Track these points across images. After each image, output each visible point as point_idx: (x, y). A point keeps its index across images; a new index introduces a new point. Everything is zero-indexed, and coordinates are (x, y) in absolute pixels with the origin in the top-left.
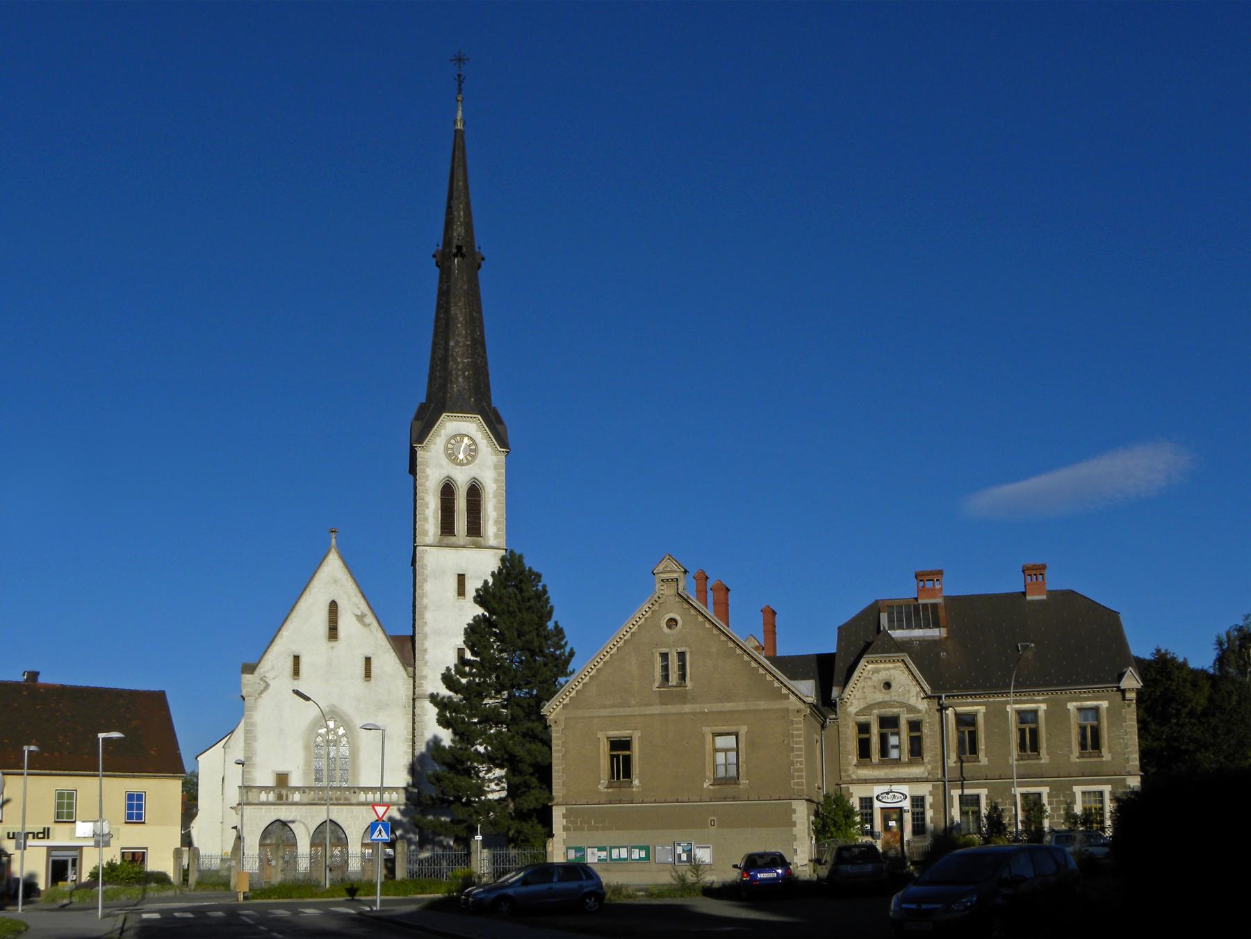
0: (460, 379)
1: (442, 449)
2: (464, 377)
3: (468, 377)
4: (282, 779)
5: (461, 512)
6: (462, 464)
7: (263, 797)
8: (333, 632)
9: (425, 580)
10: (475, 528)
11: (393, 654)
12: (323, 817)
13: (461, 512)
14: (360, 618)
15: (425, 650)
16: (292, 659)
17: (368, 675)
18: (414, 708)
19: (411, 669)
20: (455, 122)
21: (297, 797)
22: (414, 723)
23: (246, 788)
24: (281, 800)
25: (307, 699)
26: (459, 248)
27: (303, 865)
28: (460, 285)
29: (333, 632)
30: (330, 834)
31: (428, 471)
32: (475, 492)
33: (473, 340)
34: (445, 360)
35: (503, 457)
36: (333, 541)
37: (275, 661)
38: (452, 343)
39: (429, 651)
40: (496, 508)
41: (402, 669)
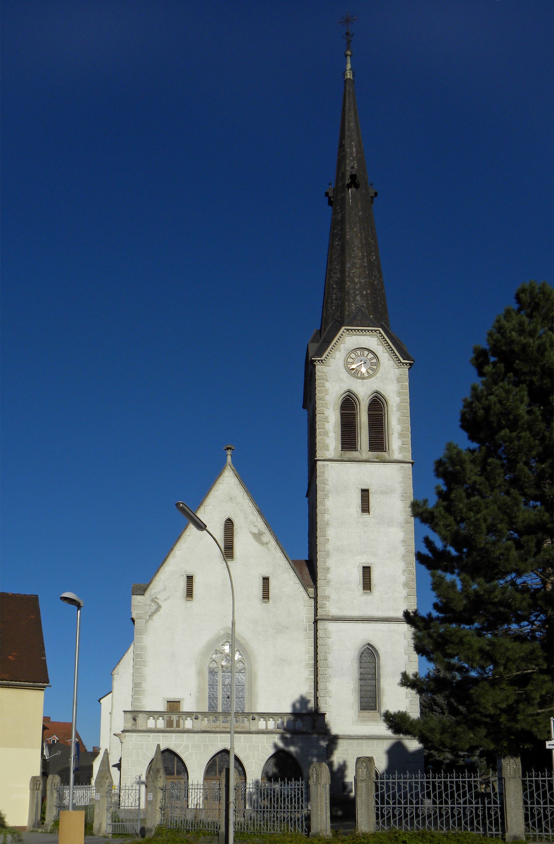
0: (358, 298)
1: (341, 364)
2: (362, 296)
3: (367, 295)
4: (173, 706)
5: (363, 427)
6: (363, 378)
7: (151, 723)
9: (326, 496)
10: (378, 443)
11: (292, 574)
13: (363, 427)
14: (257, 536)
15: (328, 569)
16: (185, 579)
17: (266, 596)
18: (316, 631)
19: (311, 590)
20: (344, 74)
21: (188, 724)
23: (134, 714)
24: (172, 727)
26: (353, 177)
27: (196, 799)
30: (222, 764)
31: (328, 385)
32: (377, 405)
33: (369, 262)
34: (342, 282)
35: (405, 370)
36: (229, 458)
37: (167, 580)
38: (348, 265)
40: (400, 422)
41: (302, 589)
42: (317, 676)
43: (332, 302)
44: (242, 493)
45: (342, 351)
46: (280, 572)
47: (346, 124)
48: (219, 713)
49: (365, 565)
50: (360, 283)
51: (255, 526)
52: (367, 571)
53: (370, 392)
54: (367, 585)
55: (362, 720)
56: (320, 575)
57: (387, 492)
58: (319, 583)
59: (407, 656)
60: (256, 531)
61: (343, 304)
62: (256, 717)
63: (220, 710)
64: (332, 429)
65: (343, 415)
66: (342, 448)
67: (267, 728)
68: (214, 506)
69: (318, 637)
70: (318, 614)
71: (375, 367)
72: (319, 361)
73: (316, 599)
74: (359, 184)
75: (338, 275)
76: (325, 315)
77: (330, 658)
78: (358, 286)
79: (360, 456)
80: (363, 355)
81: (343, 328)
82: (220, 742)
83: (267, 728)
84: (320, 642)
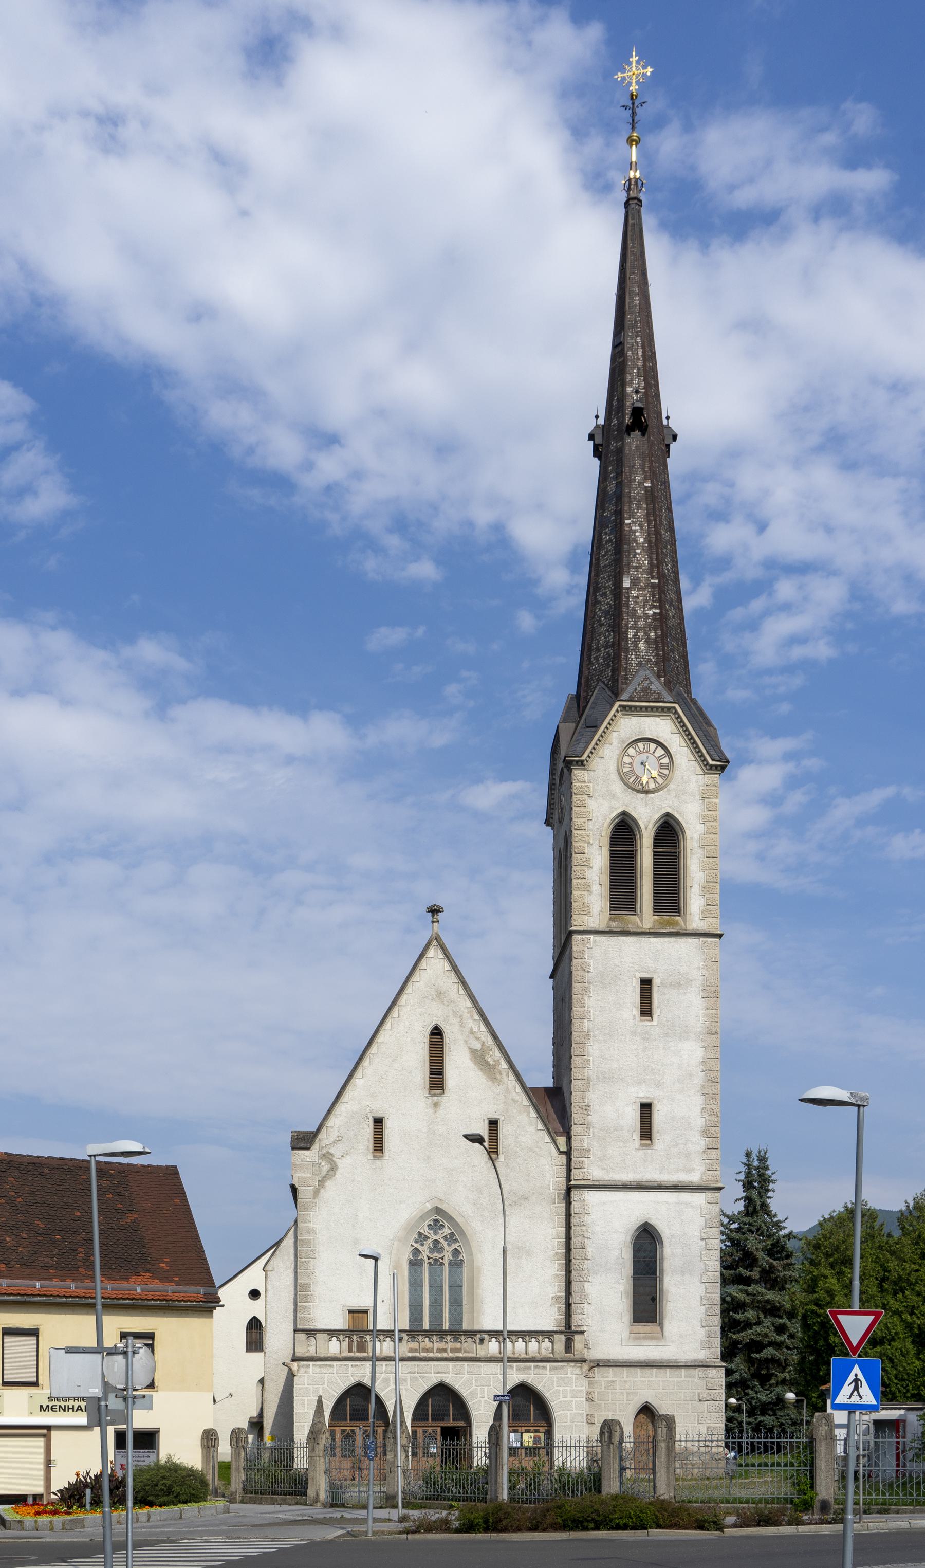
0: (642, 645)
1: (612, 767)
8: (437, 1078)
10: (669, 899)
12: (434, 1380)
19: (562, 1141)
22: (568, 1271)
25: (69, 1350)
26: (637, 412)
28: (639, 481)
29: (437, 1078)
31: (592, 804)
32: (669, 832)
38: (626, 583)
39: (595, 1107)
41: (547, 1139)
42: (570, 1272)
43: (598, 650)
44: (456, 986)
45: (615, 743)
46: (515, 1111)
47: (628, 300)
48: (445, 1331)
49: (645, 1101)
50: (646, 616)
51: (478, 1038)
52: (646, 1109)
53: (657, 816)
54: (646, 1132)
55: (637, 1338)
56: (576, 1118)
57: (679, 984)
58: (575, 1129)
59: (703, 1243)
60: (478, 1046)
61: (617, 657)
62: (486, 1336)
63: (446, 1326)
64: (597, 878)
65: (613, 855)
66: (612, 909)
67: (527, 1353)
68: (414, 1005)
69: (572, 1212)
70: (572, 1178)
71: (666, 772)
72: (577, 762)
73: (568, 1154)
74: (647, 425)
75: (610, 599)
76: (586, 672)
77: (590, 1250)
78: (641, 623)
79: (640, 924)
80: (648, 751)
81: (618, 704)
82: (360, 1373)
83: (527, 1353)
84: (575, 1220)
